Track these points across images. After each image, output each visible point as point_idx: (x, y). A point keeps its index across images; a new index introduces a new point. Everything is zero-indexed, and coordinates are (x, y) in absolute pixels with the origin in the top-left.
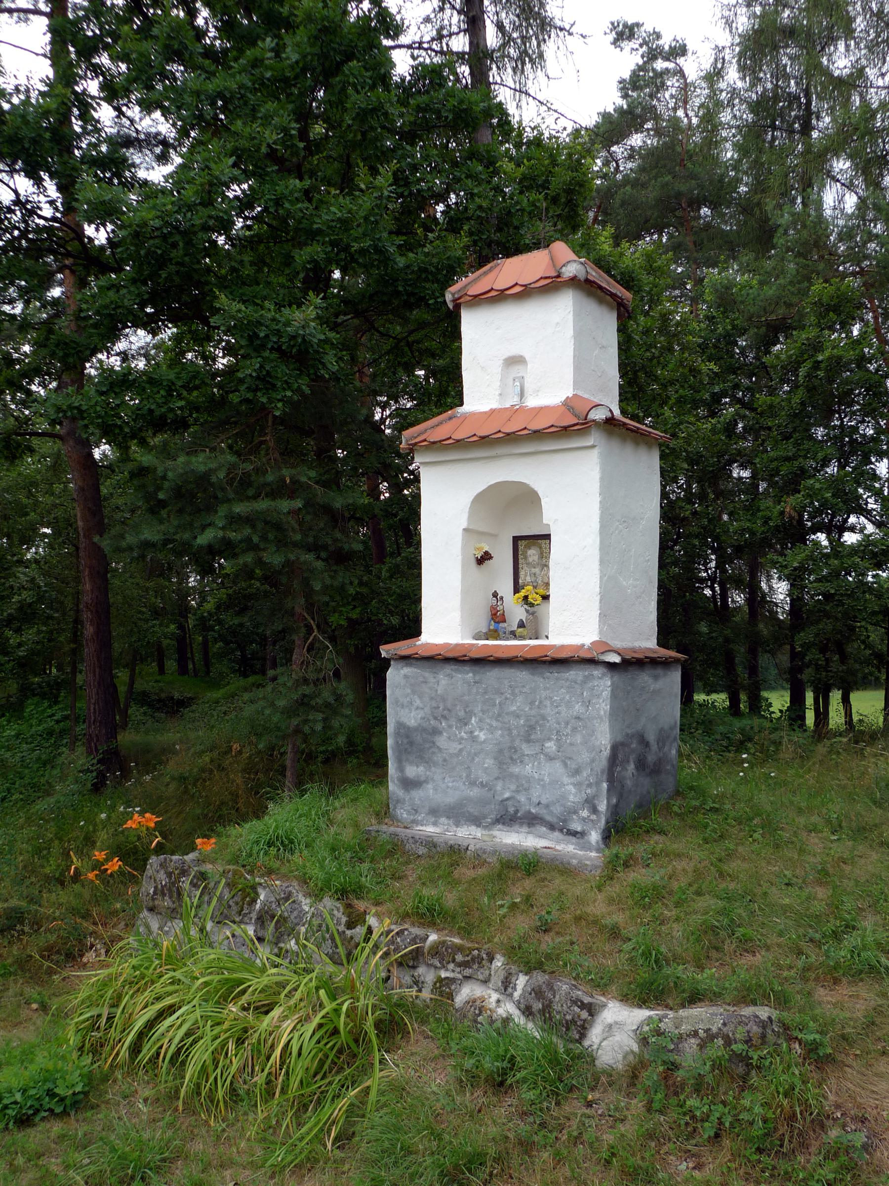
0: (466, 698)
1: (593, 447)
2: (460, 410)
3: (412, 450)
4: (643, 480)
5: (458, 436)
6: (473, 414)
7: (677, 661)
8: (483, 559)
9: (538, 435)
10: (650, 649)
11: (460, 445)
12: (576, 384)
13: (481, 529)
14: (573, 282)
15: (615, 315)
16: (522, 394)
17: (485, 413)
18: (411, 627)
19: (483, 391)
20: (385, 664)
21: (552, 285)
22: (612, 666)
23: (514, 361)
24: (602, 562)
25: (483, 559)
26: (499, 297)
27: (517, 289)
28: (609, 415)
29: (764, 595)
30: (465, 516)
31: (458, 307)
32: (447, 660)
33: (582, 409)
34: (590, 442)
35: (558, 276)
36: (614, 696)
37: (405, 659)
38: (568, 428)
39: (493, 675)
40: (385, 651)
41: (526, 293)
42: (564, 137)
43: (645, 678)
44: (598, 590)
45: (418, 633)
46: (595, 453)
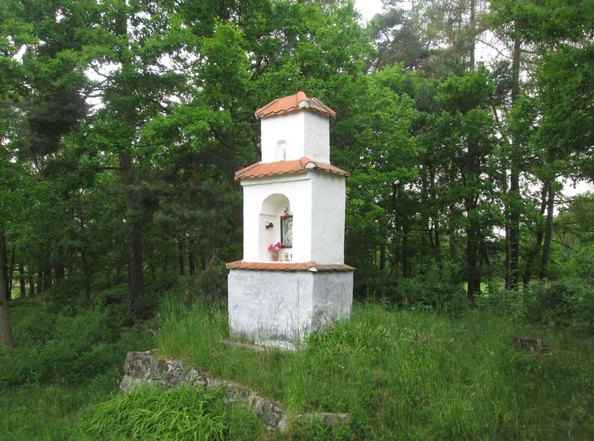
0: (258, 286)
1: (309, 179)
2: (260, 163)
3: (240, 180)
4: (336, 194)
5: (256, 174)
6: (265, 164)
7: (350, 270)
8: (270, 226)
9: (287, 174)
10: (340, 266)
11: (257, 178)
12: (306, 152)
13: (270, 214)
14: (304, 109)
15: (328, 122)
16: (285, 156)
17: (278, 163)
18: (237, 254)
19: (270, 153)
20: (228, 271)
21: (296, 111)
22: (314, 273)
23: (282, 142)
24: (313, 228)
25: (270, 226)
26: (275, 115)
27: (282, 112)
28: (315, 166)
29: (496, 242)
30: (261, 208)
31: (260, 119)
32: (251, 270)
33: (304, 162)
34: (307, 177)
35: (298, 107)
36: (315, 286)
37: (235, 269)
38: (298, 171)
39: (274, 274)
40: (228, 265)
41: (286, 114)
42: (398, 10)
43: (332, 277)
44: (311, 240)
45: (242, 258)
46: (310, 182)
